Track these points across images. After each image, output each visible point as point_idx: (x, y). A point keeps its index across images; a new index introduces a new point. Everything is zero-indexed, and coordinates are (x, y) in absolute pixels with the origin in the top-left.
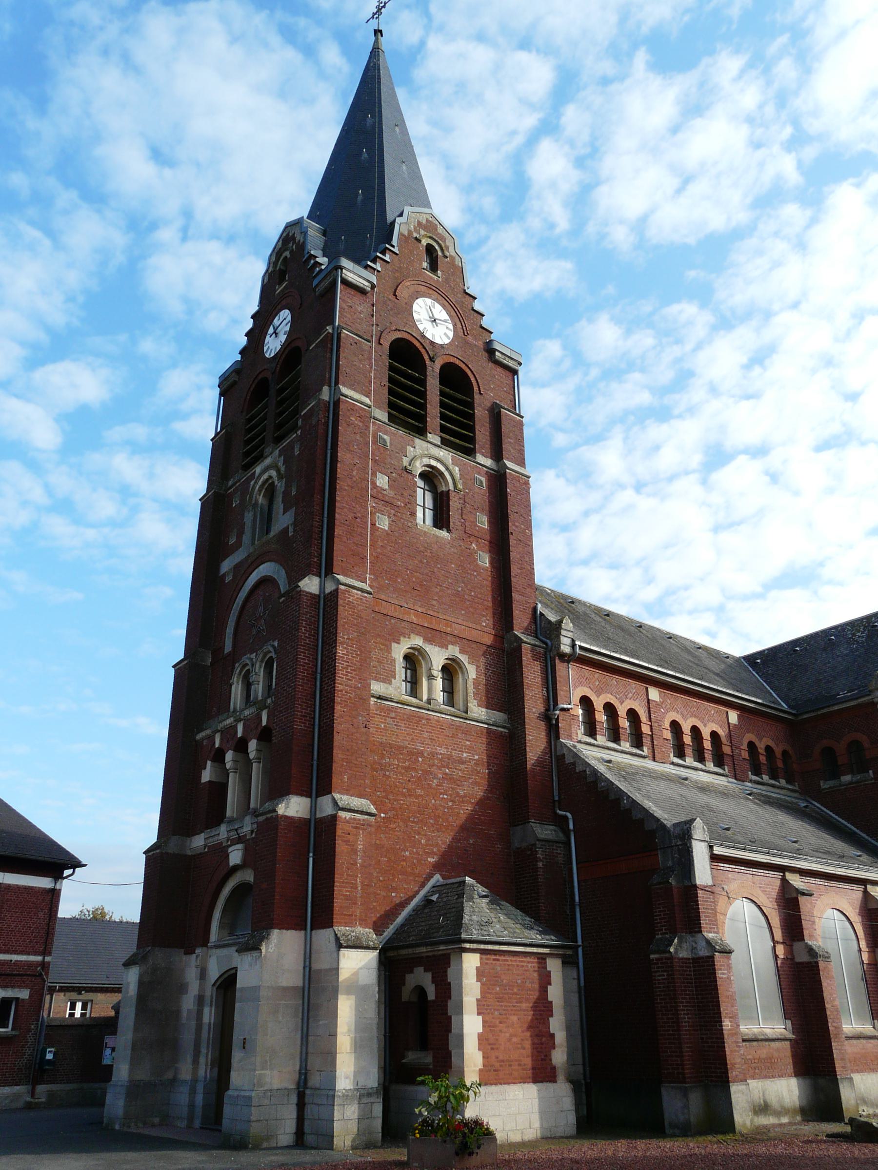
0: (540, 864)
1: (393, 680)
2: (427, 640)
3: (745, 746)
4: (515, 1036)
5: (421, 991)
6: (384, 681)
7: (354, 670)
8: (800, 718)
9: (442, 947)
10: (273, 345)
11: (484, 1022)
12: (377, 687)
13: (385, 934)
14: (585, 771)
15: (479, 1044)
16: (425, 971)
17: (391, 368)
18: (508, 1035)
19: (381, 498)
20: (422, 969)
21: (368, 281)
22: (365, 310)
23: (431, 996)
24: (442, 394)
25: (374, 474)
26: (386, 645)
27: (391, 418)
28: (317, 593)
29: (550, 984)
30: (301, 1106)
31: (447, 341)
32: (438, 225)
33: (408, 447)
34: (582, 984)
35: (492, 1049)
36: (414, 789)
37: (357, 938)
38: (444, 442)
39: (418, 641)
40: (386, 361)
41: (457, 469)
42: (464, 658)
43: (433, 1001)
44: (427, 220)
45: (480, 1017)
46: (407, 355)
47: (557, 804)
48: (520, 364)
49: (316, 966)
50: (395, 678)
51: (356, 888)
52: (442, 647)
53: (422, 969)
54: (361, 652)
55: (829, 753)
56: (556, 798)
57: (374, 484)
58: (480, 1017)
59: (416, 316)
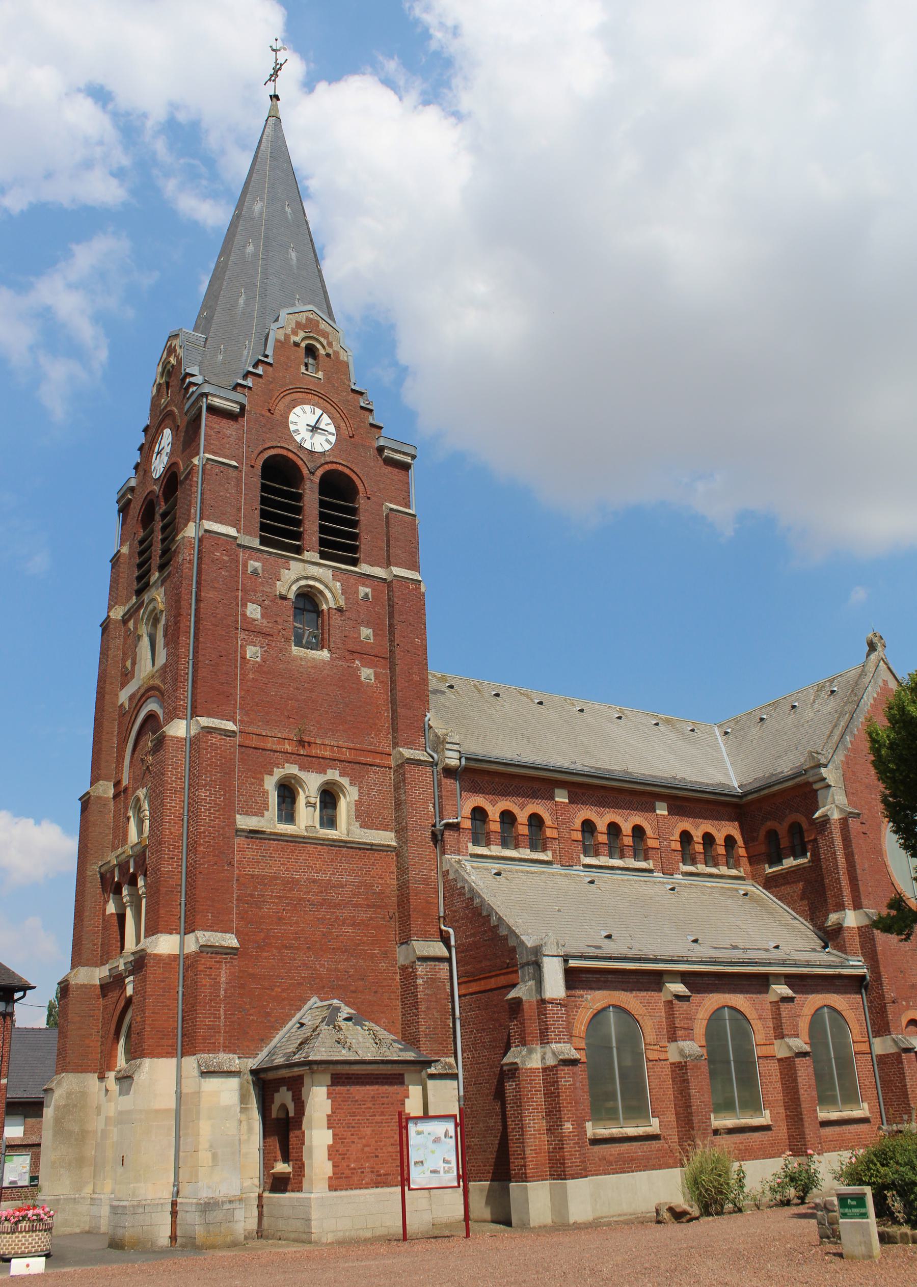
0: (420, 981)
1: (266, 813)
2: (301, 768)
3: (677, 836)
4: (369, 1146)
5: (284, 1107)
6: (255, 815)
7: (218, 811)
8: (744, 799)
9: (296, 1069)
10: (159, 465)
11: (334, 1135)
12: (244, 822)
13: (259, 1056)
14: (464, 887)
15: (329, 1155)
16: (288, 1090)
17: (264, 488)
18: (360, 1146)
19: (253, 629)
20: (285, 1088)
21: (236, 402)
22: (234, 433)
23: (291, 1114)
24: (322, 504)
25: (245, 606)
26: (258, 779)
27: (264, 541)
28: (184, 735)
29: (408, 1097)
30: (174, 1214)
31: (328, 447)
32: (321, 321)
33: (282, 570)
34: (462, 1093)
35: (343, 1159)
36: (290, 917)
37: (218, 1064)
38: (323, 556)
39: (292, 769)
40: (257, 481)
41: (338, 584)
42: (345, 781)
43: (293, 1118)
44: (307, 319)
45: (331, 1131)
46: (280, 473)
47: (442, 920)
48: (414, 457)
49: (185, 1090)
50: (268, 810)
51: (220, 1018)
52: (321, 773)
53: (285, 1088)
54: (225, 792)
55: (772, 835)
56: (442, 914)
57: (244, 615)
58: (331, 1131)
59: (292, 427)
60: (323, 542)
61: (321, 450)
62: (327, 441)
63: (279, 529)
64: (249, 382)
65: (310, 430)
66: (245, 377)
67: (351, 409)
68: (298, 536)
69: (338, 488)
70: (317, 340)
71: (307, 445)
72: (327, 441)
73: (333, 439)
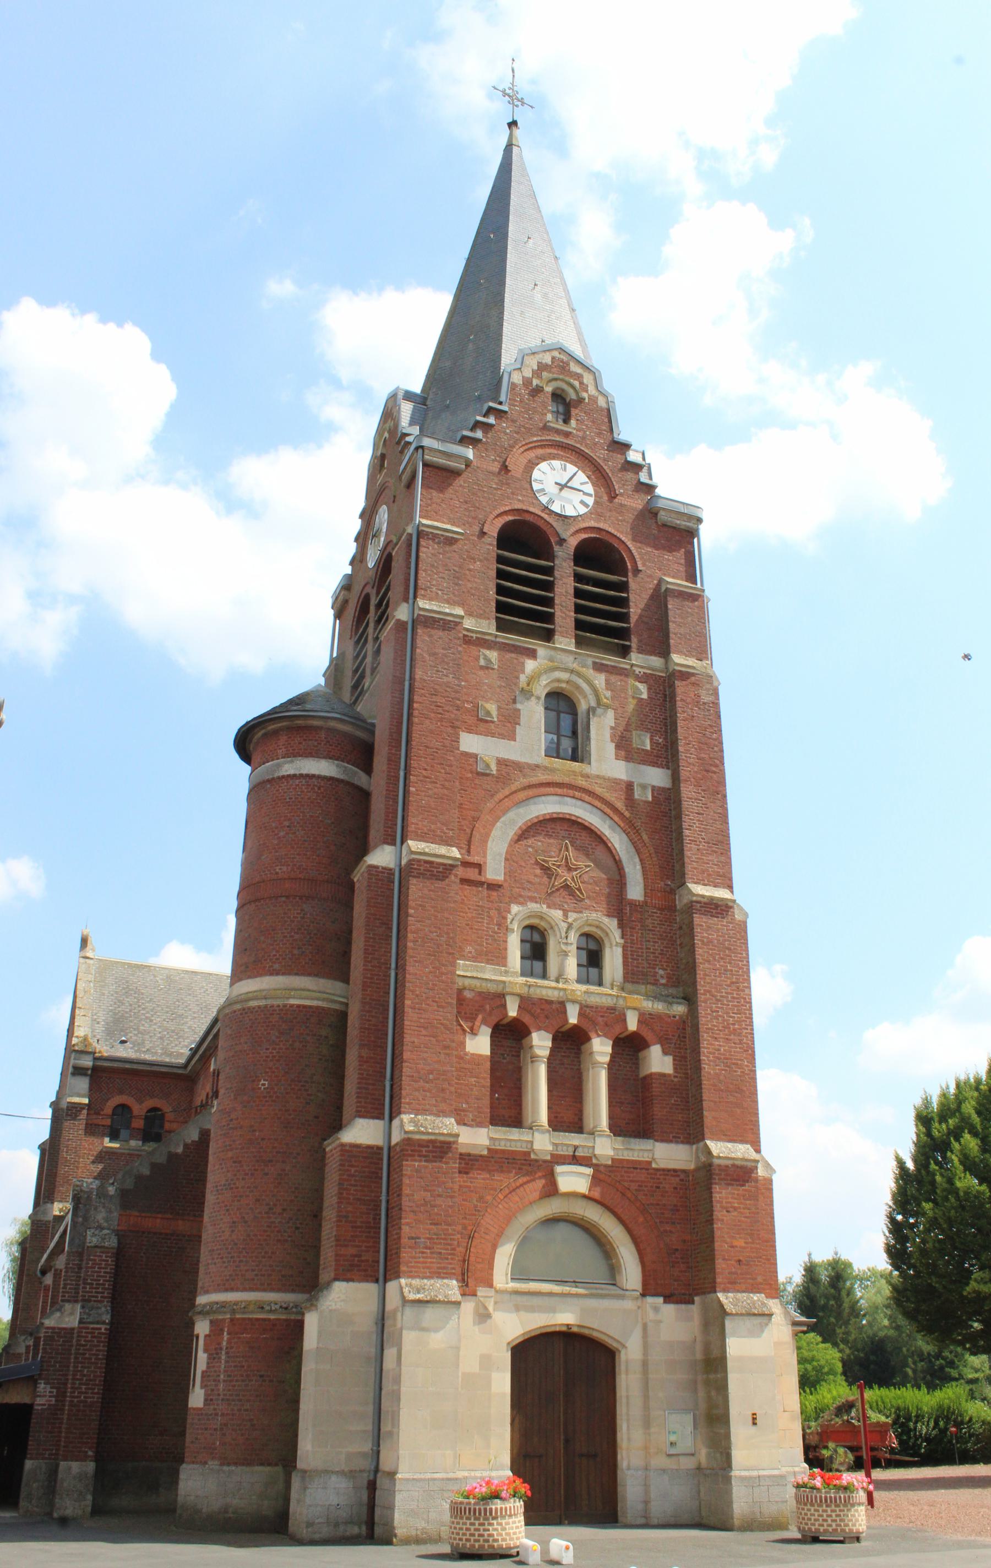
17: (500, 560)
27: (502, 626)
31: (583, 510)
46: (525, 539)
59: (536, 486)
60: (579, 625)
61: (574, 514)
62: (582, 502)
63: (523, 608)
64: (479, 434)
65: (563, 491)
66: (473, 429)
67: (613, 466)
68: (549, 618)
69: (598, 555)
70: (579, 675)
71: (556, 508)
72: (582, 502)
73: (590, 501)
